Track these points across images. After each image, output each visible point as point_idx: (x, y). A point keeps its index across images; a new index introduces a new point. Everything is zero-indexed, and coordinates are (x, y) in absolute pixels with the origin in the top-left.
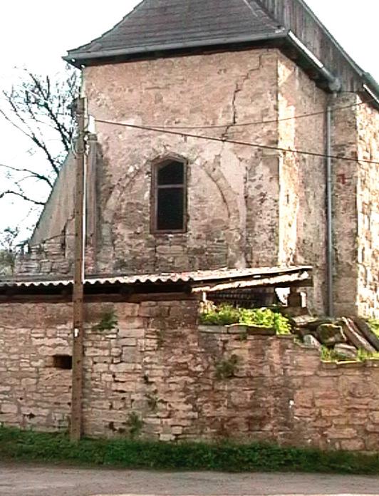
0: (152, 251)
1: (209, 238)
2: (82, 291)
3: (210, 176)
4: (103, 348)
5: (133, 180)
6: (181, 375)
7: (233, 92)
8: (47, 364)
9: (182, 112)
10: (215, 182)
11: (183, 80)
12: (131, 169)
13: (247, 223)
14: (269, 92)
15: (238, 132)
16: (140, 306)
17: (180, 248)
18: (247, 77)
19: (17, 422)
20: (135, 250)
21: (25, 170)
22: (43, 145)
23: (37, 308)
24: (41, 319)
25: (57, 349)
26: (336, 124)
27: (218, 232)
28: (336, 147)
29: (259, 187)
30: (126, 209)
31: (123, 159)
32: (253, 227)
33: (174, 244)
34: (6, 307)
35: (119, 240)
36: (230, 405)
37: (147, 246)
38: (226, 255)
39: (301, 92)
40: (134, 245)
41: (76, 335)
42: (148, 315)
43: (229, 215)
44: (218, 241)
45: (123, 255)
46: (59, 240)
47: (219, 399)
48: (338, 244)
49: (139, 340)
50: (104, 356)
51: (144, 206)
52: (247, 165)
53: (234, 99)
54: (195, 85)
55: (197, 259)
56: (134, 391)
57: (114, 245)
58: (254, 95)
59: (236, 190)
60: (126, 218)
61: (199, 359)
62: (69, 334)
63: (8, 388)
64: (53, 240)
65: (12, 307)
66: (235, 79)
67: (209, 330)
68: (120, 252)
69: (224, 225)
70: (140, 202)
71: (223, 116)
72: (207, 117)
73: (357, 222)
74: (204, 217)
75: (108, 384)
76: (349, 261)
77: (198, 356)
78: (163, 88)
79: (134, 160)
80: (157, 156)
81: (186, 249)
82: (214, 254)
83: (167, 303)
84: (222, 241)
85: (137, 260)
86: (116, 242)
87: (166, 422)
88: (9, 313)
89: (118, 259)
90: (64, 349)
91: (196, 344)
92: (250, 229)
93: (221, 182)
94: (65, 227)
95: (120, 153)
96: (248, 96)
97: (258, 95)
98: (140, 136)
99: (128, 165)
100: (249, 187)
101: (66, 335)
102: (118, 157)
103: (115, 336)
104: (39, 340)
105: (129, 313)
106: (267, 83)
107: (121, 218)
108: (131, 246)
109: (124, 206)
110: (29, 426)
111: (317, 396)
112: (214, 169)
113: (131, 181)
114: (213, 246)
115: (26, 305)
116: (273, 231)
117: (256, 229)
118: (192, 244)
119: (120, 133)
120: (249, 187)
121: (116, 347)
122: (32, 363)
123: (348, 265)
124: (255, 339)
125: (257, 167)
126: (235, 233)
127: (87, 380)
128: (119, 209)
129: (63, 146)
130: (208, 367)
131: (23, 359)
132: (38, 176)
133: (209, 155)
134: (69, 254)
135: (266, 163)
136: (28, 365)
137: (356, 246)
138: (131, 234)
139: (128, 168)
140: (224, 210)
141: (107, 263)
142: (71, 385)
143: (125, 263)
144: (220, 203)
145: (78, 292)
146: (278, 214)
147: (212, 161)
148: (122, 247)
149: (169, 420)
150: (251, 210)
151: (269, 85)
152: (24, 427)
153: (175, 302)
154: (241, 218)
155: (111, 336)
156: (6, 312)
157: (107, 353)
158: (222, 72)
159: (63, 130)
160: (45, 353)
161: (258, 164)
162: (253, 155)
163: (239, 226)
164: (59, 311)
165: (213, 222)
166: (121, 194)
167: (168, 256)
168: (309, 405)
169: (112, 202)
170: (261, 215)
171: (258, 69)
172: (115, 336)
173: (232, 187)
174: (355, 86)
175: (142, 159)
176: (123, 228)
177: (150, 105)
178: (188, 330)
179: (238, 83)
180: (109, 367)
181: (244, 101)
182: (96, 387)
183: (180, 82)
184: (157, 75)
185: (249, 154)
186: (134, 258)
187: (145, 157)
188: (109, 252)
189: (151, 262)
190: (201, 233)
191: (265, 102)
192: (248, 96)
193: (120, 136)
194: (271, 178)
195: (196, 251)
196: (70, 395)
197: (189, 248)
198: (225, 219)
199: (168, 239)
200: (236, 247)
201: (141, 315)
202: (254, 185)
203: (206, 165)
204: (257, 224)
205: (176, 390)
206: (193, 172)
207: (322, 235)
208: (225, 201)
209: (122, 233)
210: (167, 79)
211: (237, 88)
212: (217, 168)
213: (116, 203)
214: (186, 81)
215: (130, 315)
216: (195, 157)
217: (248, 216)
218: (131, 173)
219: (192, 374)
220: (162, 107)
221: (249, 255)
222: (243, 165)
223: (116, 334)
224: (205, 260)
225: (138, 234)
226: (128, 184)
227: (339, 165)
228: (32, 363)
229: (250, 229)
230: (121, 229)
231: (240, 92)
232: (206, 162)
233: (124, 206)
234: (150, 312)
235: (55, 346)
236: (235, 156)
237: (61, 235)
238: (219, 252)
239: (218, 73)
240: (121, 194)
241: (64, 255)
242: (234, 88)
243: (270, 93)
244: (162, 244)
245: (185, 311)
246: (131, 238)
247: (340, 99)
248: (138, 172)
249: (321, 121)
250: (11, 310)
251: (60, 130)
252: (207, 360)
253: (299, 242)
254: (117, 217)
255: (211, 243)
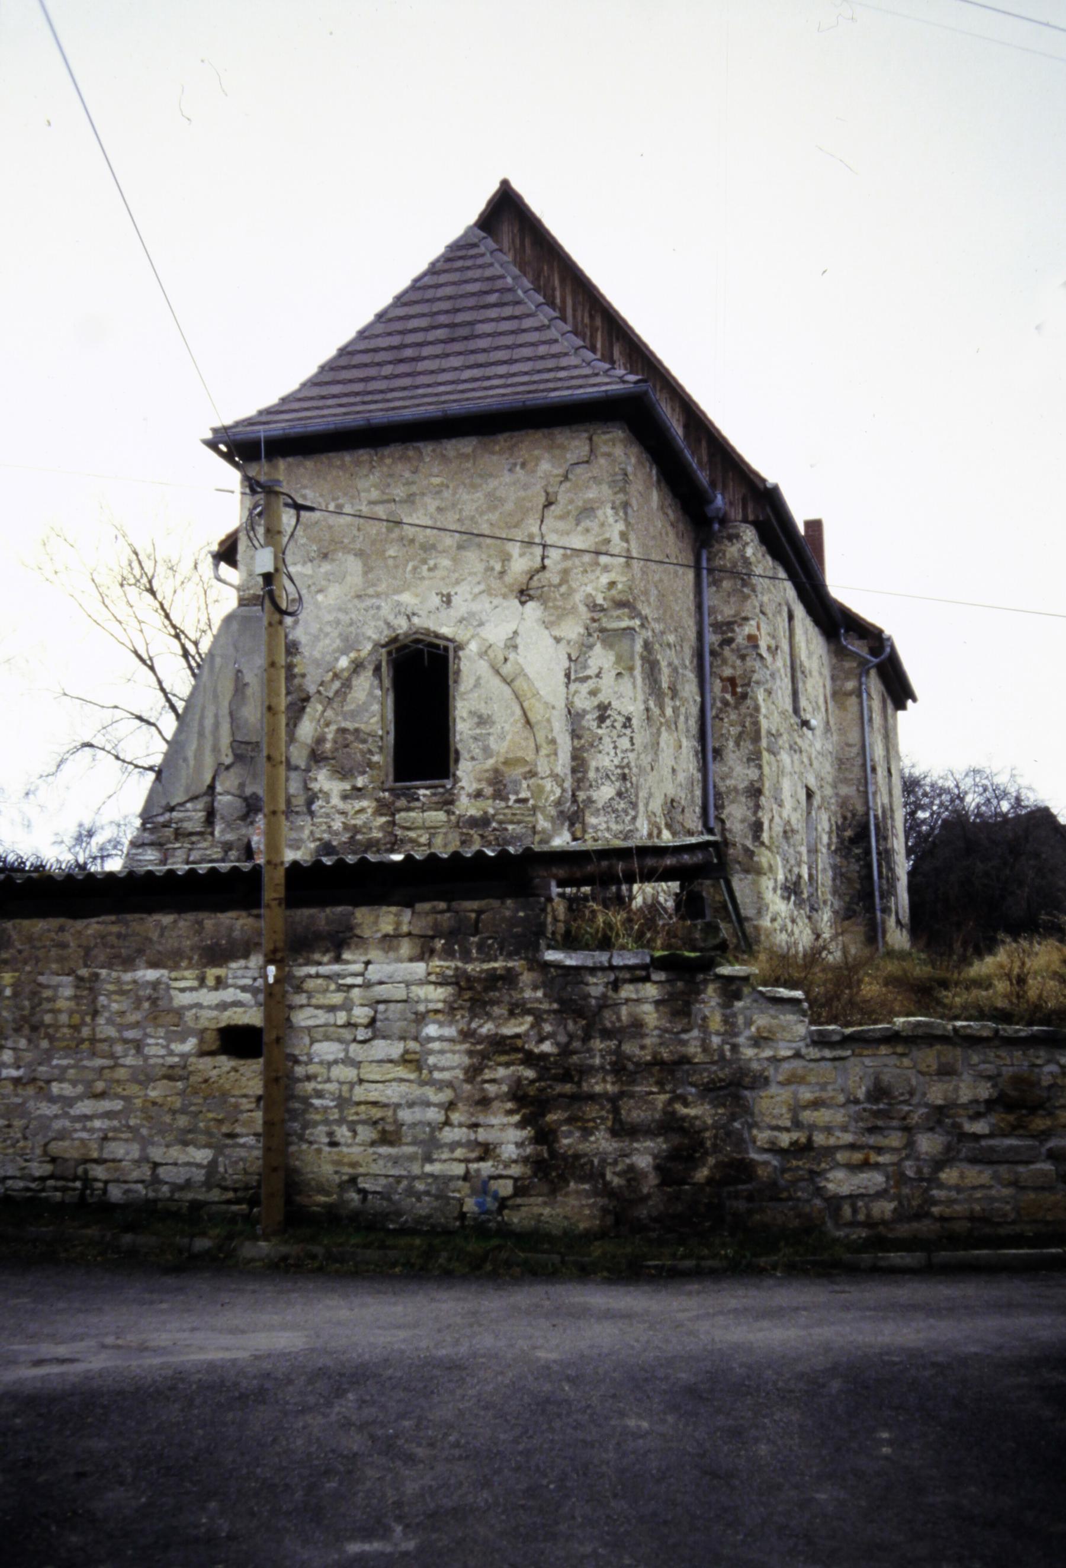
0: (388, 822)
1: (499, 795)
2: (282, 881)
3: (498, 672)
4: (332, 1009)
5: (347, 685)
6: (507, 1065)
7: (541, 507)
8: (206, 1048)
9: (440, 548)
10: (509, 684)
11: (442, 484)
12: (344, 662)
13: (574, 764)
14: (610, 505)
15: (550, 585)
16: (413, 913)
17: (441, 816)
18: (566, 478)
19: (137, 1182)
20: (353, 822)
21: (116, 707)
22: (149, 662)
23: (181, 924)
24: (192, 949)
25: (227, 1013)
26: (716, 583)
27: (516, 783)
28: (717, 627)
29: (593, 693)
30: (335, 742)
31: (327, 641)
32: (586, 772)
33: (430, 809)
34: (113, 923)
35: (320, 803)
36: (617, 1127)
37: (378, 812)
38: (534, 827)
39: (660, 514)
40: (352, 813)
41: (271, 980)
42: (430, 933)
43: (537, 749)
44: (518, 801)
45: (330, 833)
46: (200, 804)
47: (594, 1115)
48: (726, 811)
49: (413, 988)
50: (336, 1025)
51: (369, 734)
52: (569, 651)
53: (542, 521)
54: (464, 495)
55: (476, 837)
56: (403, 1102)
57: (311, 813)
58: (580, 513)
59: (551, 699)
60: (334, 758)
61: (548, 1028)
62: (255, 979)
63: (118, 1105)
64: (189, 805)
65: (126, 924)
66: (544, 483)
67: (569, 962)
68: (324, 827)
69: (527, 769)
70: (362, 726)
71: (522, 555)
72: (489, 556)
73: (760, 767)
74: (487, 751)
75: (345, 1088)
76: (749, 843)
77: (545, 1021)
78: (401, 502)
79: (348, 645)
80: (394, 635)
81: (453, 818)
82: (510, 827)
83: (475, 905)
84: (525, 801)
85: (359, 842)
86: (314, 807)
87: (478, 1170)
88: (119, 936)
89: (320, 840)
90: (245, 1012)
91: (540, 994)
92: (580, 775)
93: (519, 683)
94: (214, 779)
95: (321, 630)
96: (569, 513)
97: (588, 511)
98: (359, 597)
99: (337, 655)
100: (576, 692)
101: (249, 982)
102: (316, 638)
103: (359, 980)
104: (187, 994)
105: (389, 929)
106: (605, 488)
107: (326, 759)
108: (343, 813)
109: (330, 736)
110: (165, 1189)
111: (802, 1103)
112: (506, 660)
113: (343, 685)
114: (506, 811)
115: (157, 917)
116: (624, 777)
117: (591, 775)
118: (466, 807)
119: (320, 591)
120: (576, 692)
121: (362, 1005)
122: (173, 1046)
123: (746, 850)
124: (668, 981)
125: (591, 653)
126: (549, 785)
127: (299, 1080)
128: (320, 740)
129: (120, 762)
130: (568, 1043)
131: (152, 1037)
132: (140, 718)
133: (496, 633)
134: (222, 832)
135: (608, 644)
136: (163, 1052)
137: (760, 814)
138: (345, 790)
139: (337, 659)
140: (527, 738)
141: (298, 848)
142: (260, 1092)
143: (334, 847)
144: (519, 725)
145: (273, 888)
146: (633, 744)
147: (502, 645)
148: (327, 815)
149: (482, 1165)
150: (579, 737)
151: (610, 492)
152: (155, 1191)
153: (491, 901)
154: (561, 754)
155: (349, 981)
156: (110, 934)
157: (341, 1017)
158: (518, 468)
159: (182, 637)
160: (203, 1023)
161: (591, 647)
162: (582, 630)
163: (559, 770)
164: (231, 929)
165: (506, 763)
166: (324, 711)
167: (420, 832)
168: (788, 1124)
169: (306, 729)
170: (601, 747)
171: (587, 462)
172: (359, 980)
173: (541, 693)
174: (750, 511)
175: (365, 642)
176: (330, 778)
177: (378, 534)
178: (523, 962)
179: (550, 490)
180: (347, 1051)
181: (561, 525)
182: (319, 1094)
183: (437, 489)
184: (391, 476)
185: (573, 629)
186: (352, 838)
187: (369, 638)
188: (302, 827)
189: (385, 844)
190: (483, 785)
191: (602, 525)
192: (569, 513)
193: (320, 597)
194: (619, 674)
195: (475, 823)
196: (259, 1115)
197: (460, 816)
198: (530, 757)
199: (418, 799)
200: (553, 812)
201: (415, 931)
202: (584, 688)
203: (490, 652)
204: (593, 764)
205: (497, 1097)
206: (465, 666)
207: (698, 793)
208: (528, 722)
209: (326, 788)
210: (408, 483)
211: (547, 499)
212: (512, 656)
213: (316, 730)
214: (448, 487)
215: (391, 933)
216: (468, 636)
217: (574, 749)
218: (343, 670)
219: (530, 1059)
220: (402, 539)
221: (578, 826)
222: (562, 651)
223: (362, 974)
224: (492, 838)
225: (359, 790)
226: (337, 693)
227: (725, 662)
228: (173, 1046)
229: (580, 775)
230: (324, 780)
231: (553, 507)
232: (490, 646)
233: (330, 736)
234: (436, 926)
235: (223, 1006)
236: (546, 632)
237: (205, 794)
238: (519, 822)
239: (510, 470)
240: (324, 711)
241: (212, 834)
242: (542, 500)
243: (613, 508)
244: (408, 809)
245: (513, 922)
246: (345, 797)
247: (725, 534)
248: (357, 666)
249: (690, 575)
250: (123, 930)
251: (177, 636)
252: (565, 1027)
253: (666, 803)
254: (316, 757)
255: (503, 804)
